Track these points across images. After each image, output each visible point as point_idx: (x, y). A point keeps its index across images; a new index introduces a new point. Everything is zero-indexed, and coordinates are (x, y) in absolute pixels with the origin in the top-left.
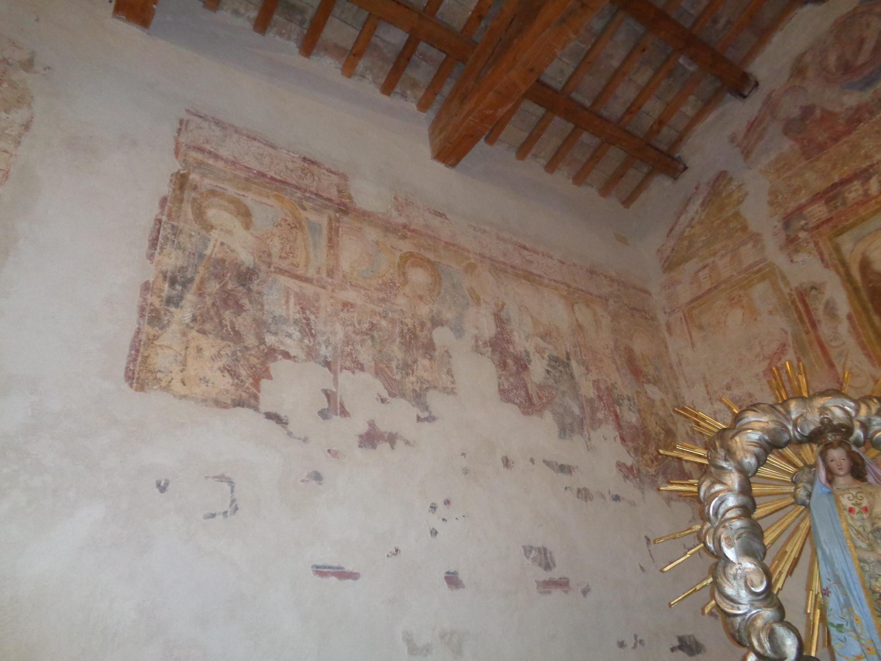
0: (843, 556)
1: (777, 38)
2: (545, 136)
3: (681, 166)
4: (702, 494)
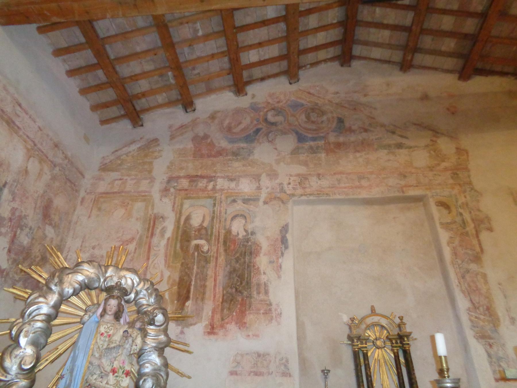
0: (82, 359)
1: (213, 96)
2: (77, 54)
3: (141, 123)
4: (29, 300)
